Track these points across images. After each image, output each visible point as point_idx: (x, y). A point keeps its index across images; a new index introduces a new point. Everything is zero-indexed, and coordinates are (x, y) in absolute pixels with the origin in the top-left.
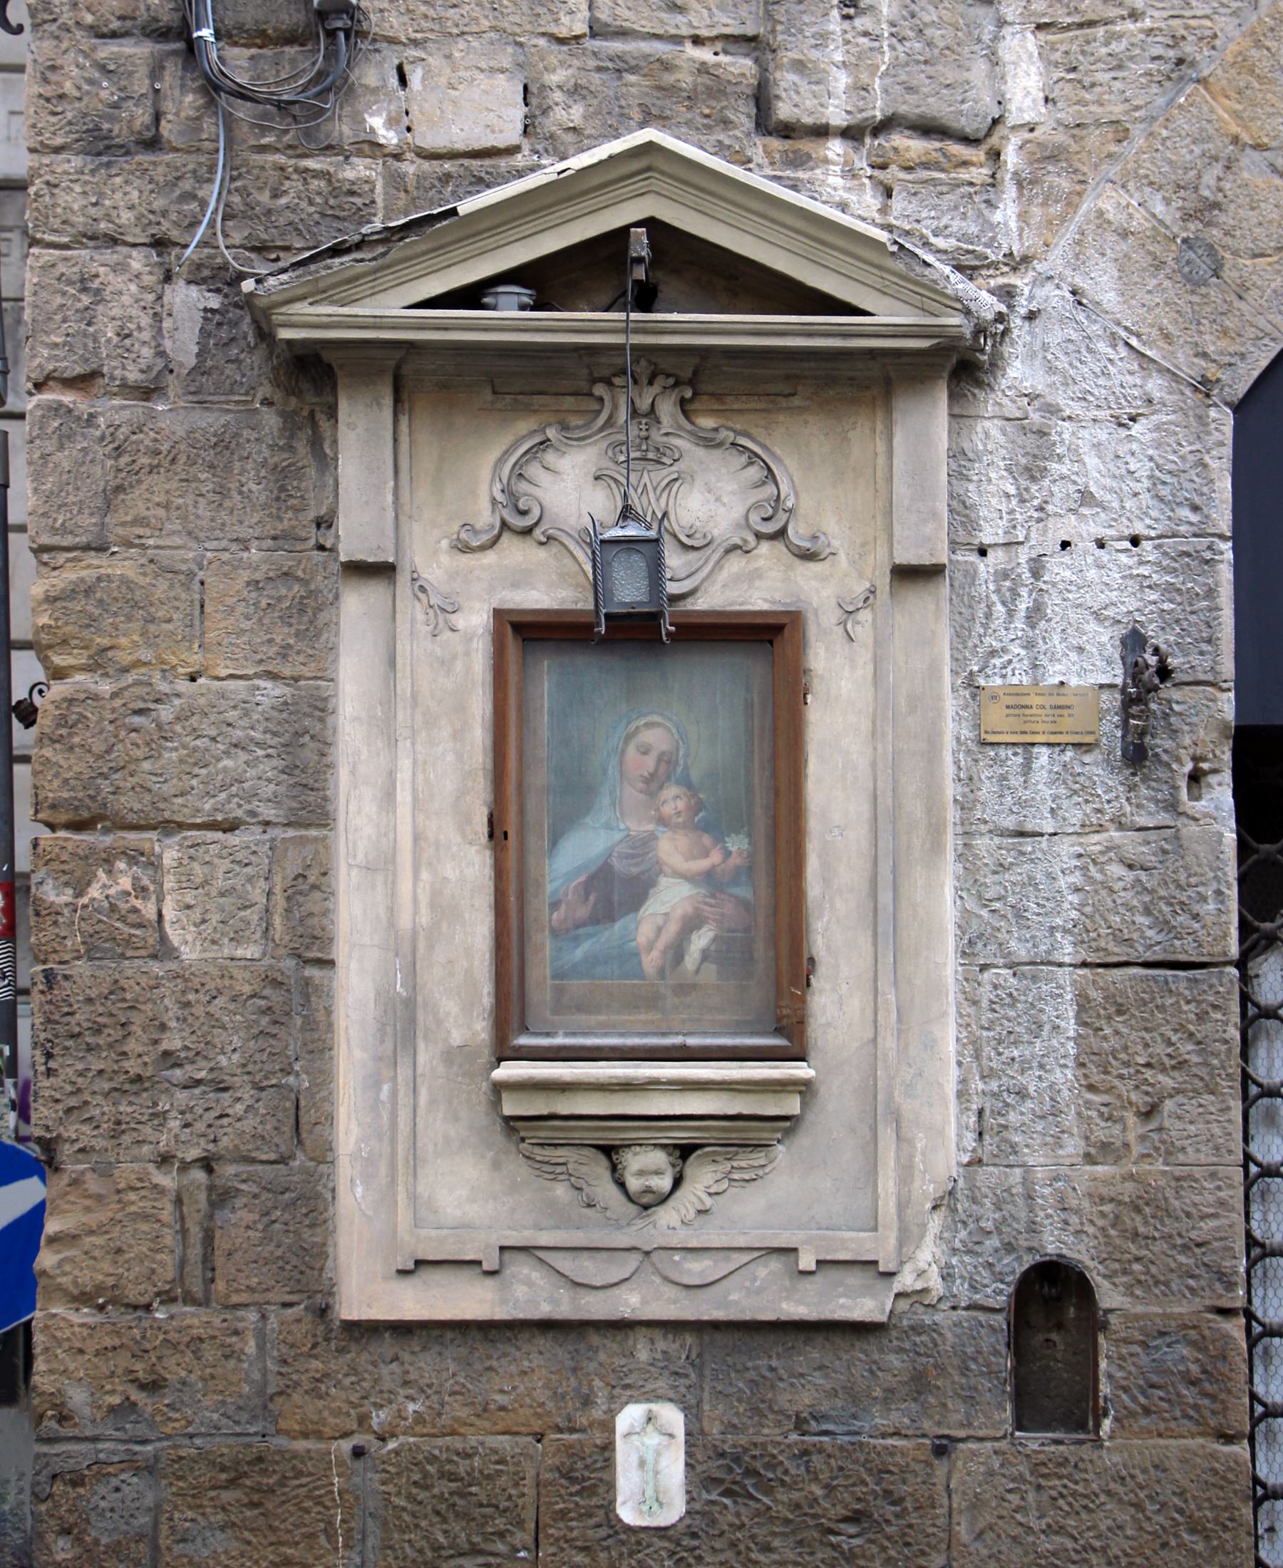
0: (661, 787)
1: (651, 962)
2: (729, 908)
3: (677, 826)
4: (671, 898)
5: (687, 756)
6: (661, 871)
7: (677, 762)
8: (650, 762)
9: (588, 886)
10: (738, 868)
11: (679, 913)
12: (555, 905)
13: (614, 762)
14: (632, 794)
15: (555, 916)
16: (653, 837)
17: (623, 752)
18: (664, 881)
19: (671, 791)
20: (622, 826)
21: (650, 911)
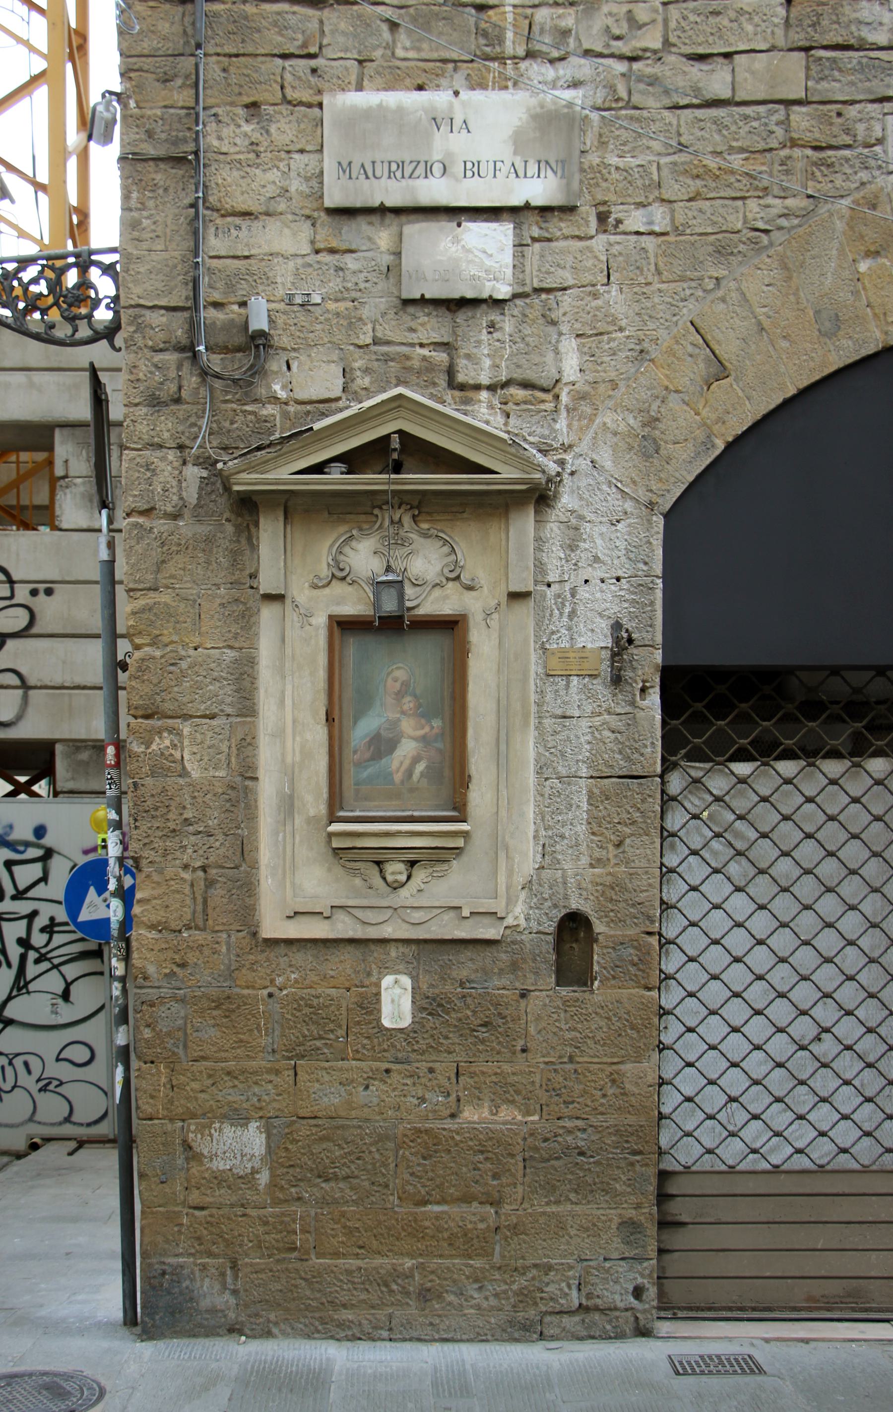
1: (398, 777)
4: (407, 749)
11: (410, 755)
12: (355, 752)
14: (390, 700)
16: (399, 720)
18: (404, 740)
19: (408, 699)
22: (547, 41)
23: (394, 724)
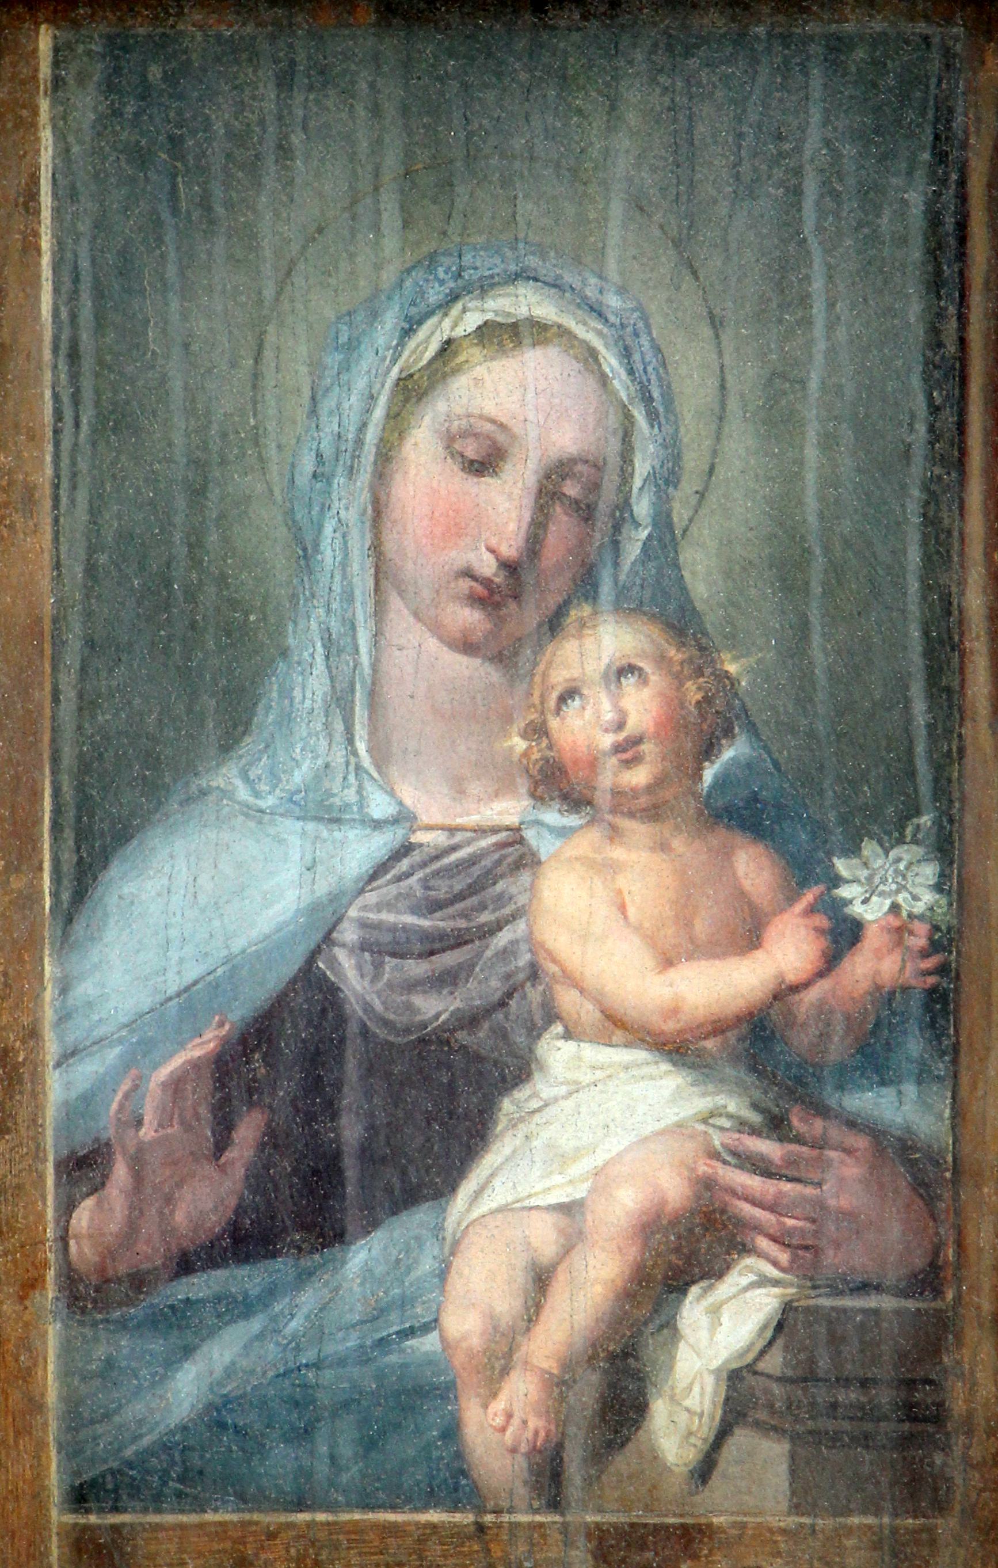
0: (554, 624)
1: (501, 1424)
2: (845, 1181)
3: (623, 801)
4: (594, 1139)
5: (667, 479)
6: (551, 1015)
7: (622, 515)
8: (504, 508)
9: (233, 1074)
10: (887, 999)
11: (626, 1202)
12: (84, 1167)
13: (348, 501)
14: (423, 659)
15: (83, 1216)
16: (516, 854)
17: (386, 456)
18: (559, 1056)
19: (605, 640)
20: (380, 806)
21: (499, 1195)
22: (529, 879)
23: (466, 898)
